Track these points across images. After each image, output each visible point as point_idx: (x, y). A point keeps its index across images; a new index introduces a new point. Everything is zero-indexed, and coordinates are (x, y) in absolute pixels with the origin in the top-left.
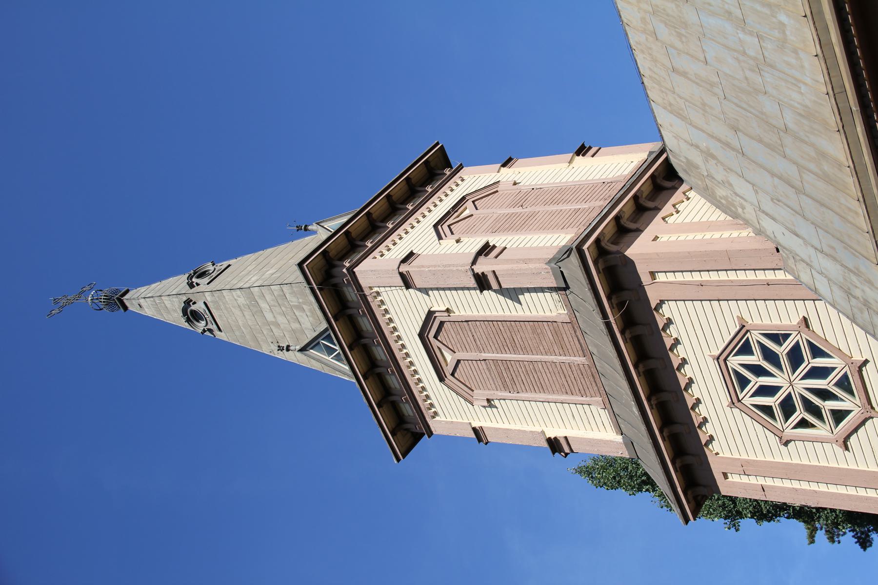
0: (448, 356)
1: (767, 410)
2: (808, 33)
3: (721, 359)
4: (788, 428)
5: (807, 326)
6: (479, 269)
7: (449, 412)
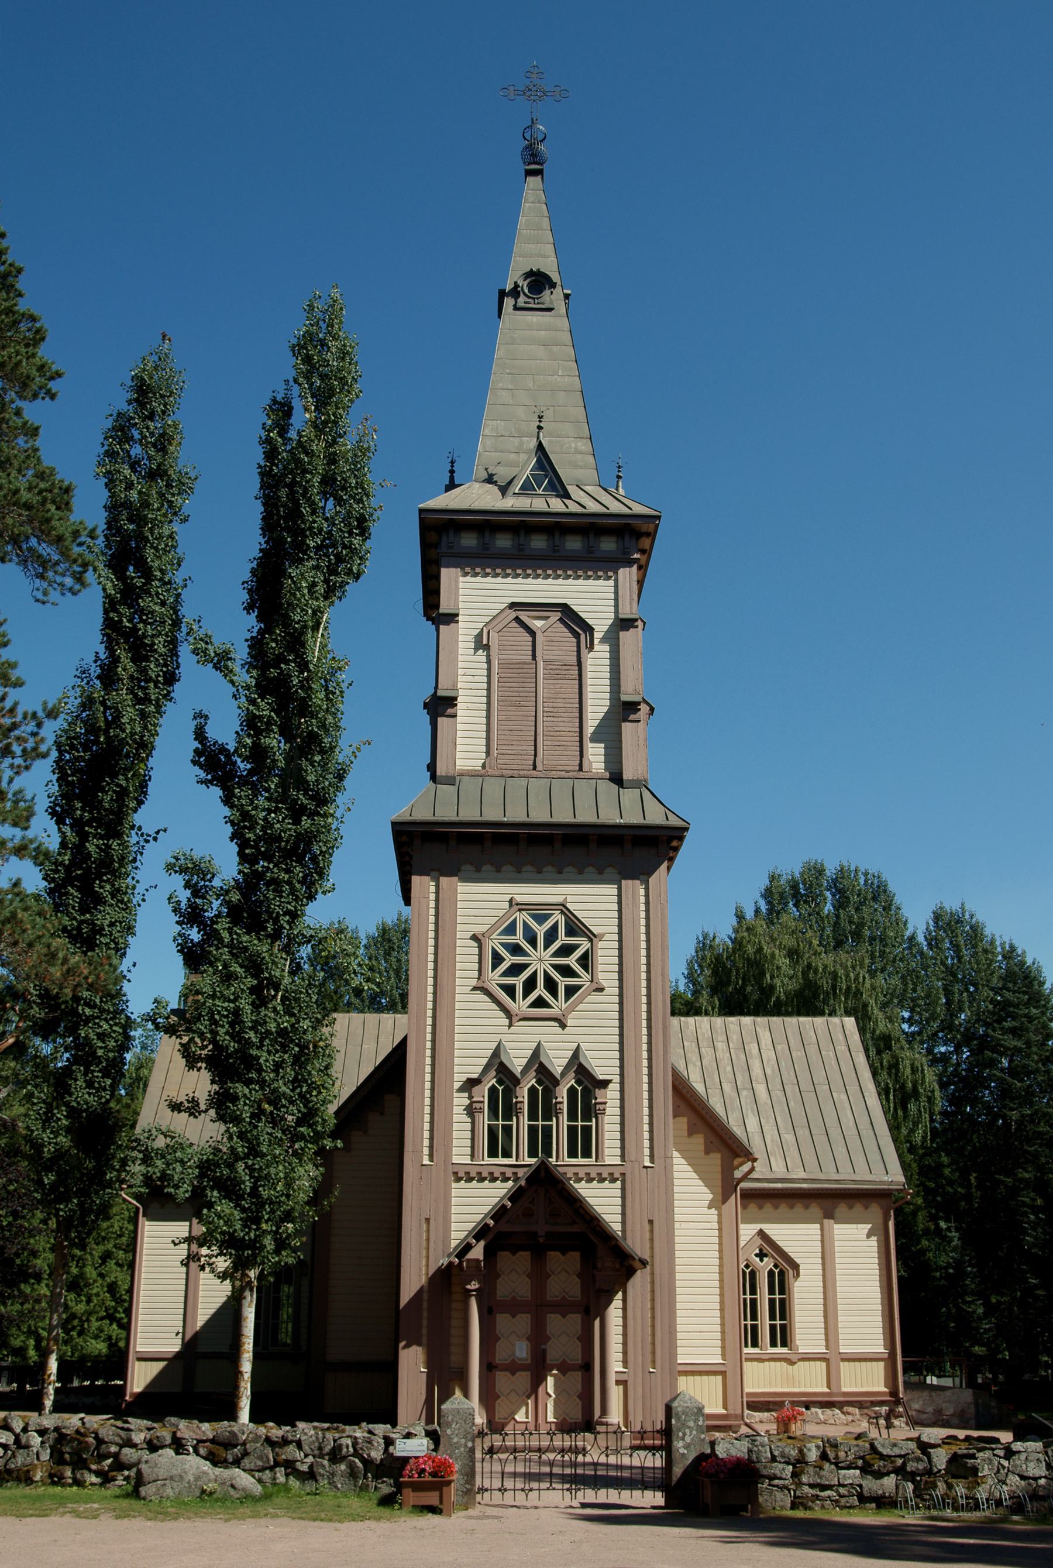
0: (538, 624)
3: (563, 908)
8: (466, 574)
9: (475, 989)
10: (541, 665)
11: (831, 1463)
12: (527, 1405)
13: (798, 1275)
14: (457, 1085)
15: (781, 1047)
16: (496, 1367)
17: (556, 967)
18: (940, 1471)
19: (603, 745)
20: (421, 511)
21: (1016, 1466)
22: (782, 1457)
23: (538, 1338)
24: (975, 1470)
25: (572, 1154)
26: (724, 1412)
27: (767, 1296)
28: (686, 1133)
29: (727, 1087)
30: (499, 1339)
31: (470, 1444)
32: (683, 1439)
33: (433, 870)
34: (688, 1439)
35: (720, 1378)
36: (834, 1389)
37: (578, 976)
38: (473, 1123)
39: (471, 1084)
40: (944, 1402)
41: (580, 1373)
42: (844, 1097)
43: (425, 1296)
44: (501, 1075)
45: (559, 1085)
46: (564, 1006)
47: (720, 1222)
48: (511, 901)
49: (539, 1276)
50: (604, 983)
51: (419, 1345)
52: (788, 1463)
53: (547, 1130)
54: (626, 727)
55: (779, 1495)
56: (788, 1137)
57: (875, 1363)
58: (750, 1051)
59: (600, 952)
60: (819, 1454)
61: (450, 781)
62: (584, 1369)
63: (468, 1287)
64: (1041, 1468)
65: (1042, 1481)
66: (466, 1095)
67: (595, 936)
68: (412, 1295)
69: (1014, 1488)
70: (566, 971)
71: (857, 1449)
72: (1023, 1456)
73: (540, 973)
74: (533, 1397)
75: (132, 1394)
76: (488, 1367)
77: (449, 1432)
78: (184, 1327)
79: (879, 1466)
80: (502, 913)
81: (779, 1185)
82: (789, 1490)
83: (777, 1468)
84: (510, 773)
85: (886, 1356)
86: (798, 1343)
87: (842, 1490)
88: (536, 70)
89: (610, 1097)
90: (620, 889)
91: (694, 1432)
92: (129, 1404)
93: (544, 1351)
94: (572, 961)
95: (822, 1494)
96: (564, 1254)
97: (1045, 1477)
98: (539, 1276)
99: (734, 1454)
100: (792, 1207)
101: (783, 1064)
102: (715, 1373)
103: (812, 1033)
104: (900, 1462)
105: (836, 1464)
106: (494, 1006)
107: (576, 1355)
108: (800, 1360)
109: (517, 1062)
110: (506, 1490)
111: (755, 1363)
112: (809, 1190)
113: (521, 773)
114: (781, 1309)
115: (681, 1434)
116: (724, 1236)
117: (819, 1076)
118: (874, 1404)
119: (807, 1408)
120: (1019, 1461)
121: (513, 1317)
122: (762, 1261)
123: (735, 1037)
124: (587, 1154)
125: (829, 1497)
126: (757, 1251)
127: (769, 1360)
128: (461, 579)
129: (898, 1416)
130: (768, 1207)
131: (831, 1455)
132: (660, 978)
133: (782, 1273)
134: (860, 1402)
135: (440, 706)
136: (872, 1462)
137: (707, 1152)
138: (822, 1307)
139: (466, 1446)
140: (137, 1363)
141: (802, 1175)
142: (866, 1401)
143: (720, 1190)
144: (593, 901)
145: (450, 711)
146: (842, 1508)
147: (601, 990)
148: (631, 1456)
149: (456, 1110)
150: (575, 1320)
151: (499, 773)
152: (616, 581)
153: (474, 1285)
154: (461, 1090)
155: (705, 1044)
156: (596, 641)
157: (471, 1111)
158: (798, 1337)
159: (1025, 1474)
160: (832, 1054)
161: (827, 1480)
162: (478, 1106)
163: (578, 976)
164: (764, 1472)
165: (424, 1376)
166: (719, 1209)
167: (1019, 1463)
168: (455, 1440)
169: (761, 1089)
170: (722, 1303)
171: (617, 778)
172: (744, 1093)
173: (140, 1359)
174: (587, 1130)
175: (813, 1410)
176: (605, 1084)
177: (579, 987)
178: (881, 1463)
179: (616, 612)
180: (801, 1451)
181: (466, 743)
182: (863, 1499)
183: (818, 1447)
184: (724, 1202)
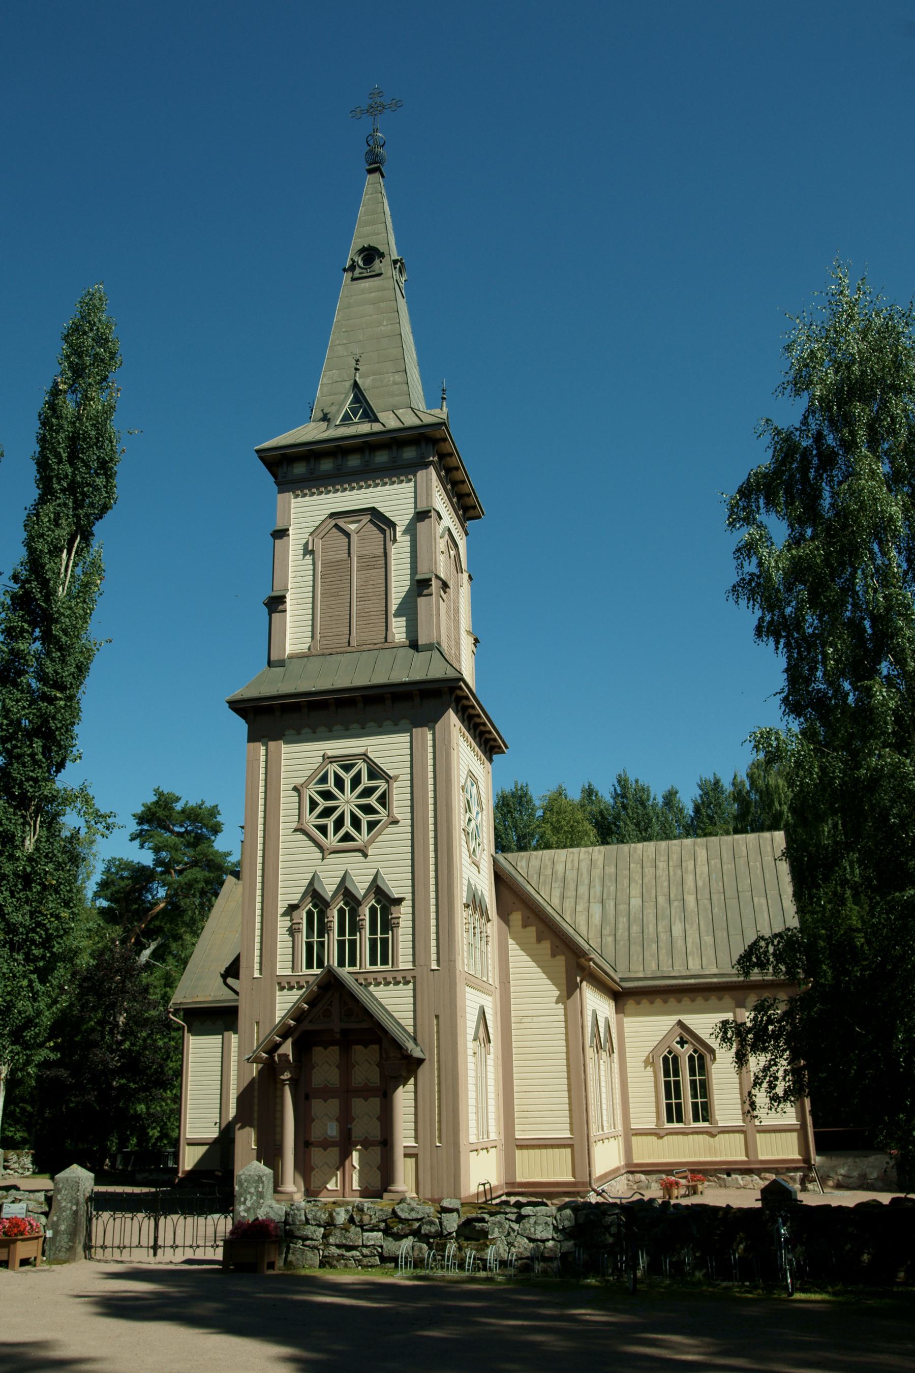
0: (353, 527)
1: (324, 780)
2: (210, 999)
3: (365, 757)
4: (311, 791)
5: (391, 823)
6: (434, 582)
7: (305, 512)
8: (297, 496)
9: (296, 830)
10: (355, 559)
11: (357, 1226)
12: (336, 1176)
13: (715, 1059)
14: (281, 911)
15: (715, 862)
16: (312, 1144)
17: (360, 807)
18: (450, 1233)
19: (404, 619)
20: (257, 451)
21: (525, 1230)
22: (315, 1220)
23: (345, 1118)
24: (484, 1234)
25: (373, 962)
26: (573, 1180)
27: (663, 1079)
28: (534, 940)
29: (661, 900)
30: (314, 1120)
31: (74, 1208)
32: (244, 1203)
33: (263, 737)
34: (248, 1204)
35: (569, 1150)
36: (752, 1158)
37: (378, 813)
38: (293, 941)
39: (292, 909)
40: (868, 1167)
41: (379, 1148)
42: (763, 901)
43: (256, 1086)
44: (346, 898)
45: (361, 905)
46: (366, 838)
47: (566, 1015)
48: (323, 756)
49: (346, 1067)
50: (398, 817)
51: (251, 1126)
52: (319, 1226)
53: (353, 943)
54: (421, 601)
55: (309, 1254)
56: (708, 939)
57: (789, 1134)
58: (687, 867)
59: (395, 791)
60: (347, 1217)
61: (281, 663)
62: (383, 1143)
63: (282, 1077)
64: (548, 1232)
65: (550, 1244)
66: (288, 918)
67: (391, 778)
68: (245, 1085)
69: (521, 1250)
70: (368, 809)
71: (381, 1213)
72: (532, 1220)
73: (347, 810)
74: (341, 1169)
75: (184, 1172)
76: (304, 1144)
77: (59, 1197)
78: (220, 1118)
79: (398, 1229)
80: (316, 766)
81: (692, 981)
82: (318, 1250)
83: (309, 1230)
84: (329, 651)
85: (798, 1127)
86: (717, 1117)
87: (365, 1251)
88: (377, 91)
89: (404, 911)
90: (411, 736)
91: (254, 1198)
92: (181, 1179)
93: (350, 1129)
94: (372, 801)
95: (348, 1254)
96: (366, 1048)
97: (553, 1239)
98: (346, 1067)
99: (272, 1217)
100: (693, 1000)
101: (714, 876)
102: (564, 1146)
103: (744, 848)
104: (416, 1225)
105: (362, 1227)
106: (310, 843)
107: (376, 1133)
108: (719, 1133)
109: (329, 888)
110: (177, 1247)
111: (681, 1137)
112: (719, 983)
113: (338, 650)
114: (702, 1089)
115: (242, 1199)
116: (569, 1026)
117: (744, 885)
118: (789, 1170)
119: (729, 1175)
120: (528, 1224)
121: (325, 1101)
122: (682, 1047)
123: (675, 857)
124: (385, 962)
125: (353, 1257)
126: (678, 1039)
127: (693, 1133)
128: (293, 501)
129: (812, 1181)
130: (686, 1001)
131: (357, 1219)
132: (444, 808)
133: (701, 1057)
134: (776, 1168)
135: (276, 603)
136: (392, 1225)
137: (554, 955)
138: (738, 1086)
139: (71, 1209)
140: (187, 1147)
141: (714, 971)
142: (782, 1168)
143: (564, 987)
144: (389, 749)
145: (281, 608)
146: (364, 1267)
147: (396, 822)
148: (132, 1219)
149: (279, 931)
150: (375, 1103)
151: (321, 652)
152: (415, 482)
153: (286, 1076)
154: (284, 915)
155: (649, 864)
156: (398, 534)
157: (292, 931)
158: (717, 1112)
159: (533, 1237)
160: (758, 864)
161: (351, 1240)
162: (296, 926)
163: (378, 813)
164: (298, 1233)
165: (255, 1152)
166: (564, 1003)
167: (528, 1226)
168: (63, 1204)
169: (690, 900)
170: (569, 1085)
171: (414, 645)
172: (675, 904)
173: (189, 1144)
174: (385, 942)
175: (734, 1176)
176: (399, 901)
177: (378, 822)
178: (400, 1226)
179: (416, 508)
180: (331, 1215)
181: (295, 633)
182: (384, 1259)
183: (347, 1211)
184: (569, 997)
